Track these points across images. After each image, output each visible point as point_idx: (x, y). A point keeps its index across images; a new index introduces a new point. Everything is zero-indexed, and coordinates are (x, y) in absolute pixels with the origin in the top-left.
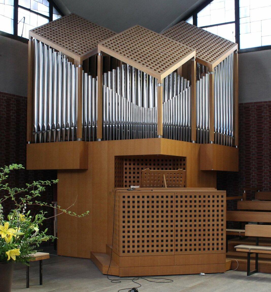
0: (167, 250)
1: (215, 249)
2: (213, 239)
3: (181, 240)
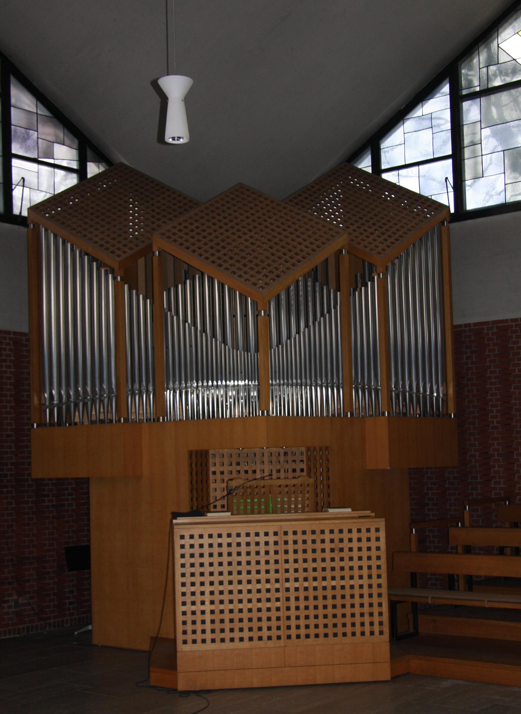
0: (270, 638)
1: (367, 633)
2: (362, 615)
3: (298, 618)
